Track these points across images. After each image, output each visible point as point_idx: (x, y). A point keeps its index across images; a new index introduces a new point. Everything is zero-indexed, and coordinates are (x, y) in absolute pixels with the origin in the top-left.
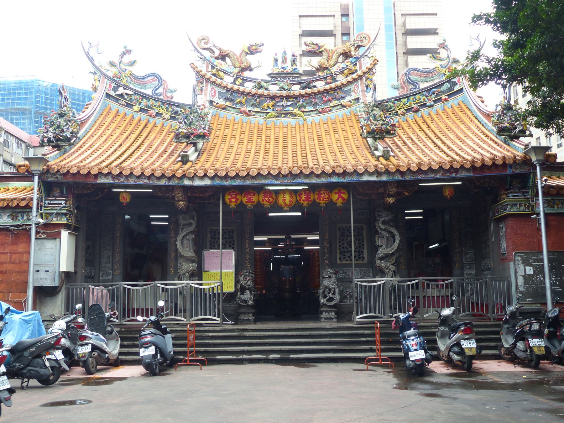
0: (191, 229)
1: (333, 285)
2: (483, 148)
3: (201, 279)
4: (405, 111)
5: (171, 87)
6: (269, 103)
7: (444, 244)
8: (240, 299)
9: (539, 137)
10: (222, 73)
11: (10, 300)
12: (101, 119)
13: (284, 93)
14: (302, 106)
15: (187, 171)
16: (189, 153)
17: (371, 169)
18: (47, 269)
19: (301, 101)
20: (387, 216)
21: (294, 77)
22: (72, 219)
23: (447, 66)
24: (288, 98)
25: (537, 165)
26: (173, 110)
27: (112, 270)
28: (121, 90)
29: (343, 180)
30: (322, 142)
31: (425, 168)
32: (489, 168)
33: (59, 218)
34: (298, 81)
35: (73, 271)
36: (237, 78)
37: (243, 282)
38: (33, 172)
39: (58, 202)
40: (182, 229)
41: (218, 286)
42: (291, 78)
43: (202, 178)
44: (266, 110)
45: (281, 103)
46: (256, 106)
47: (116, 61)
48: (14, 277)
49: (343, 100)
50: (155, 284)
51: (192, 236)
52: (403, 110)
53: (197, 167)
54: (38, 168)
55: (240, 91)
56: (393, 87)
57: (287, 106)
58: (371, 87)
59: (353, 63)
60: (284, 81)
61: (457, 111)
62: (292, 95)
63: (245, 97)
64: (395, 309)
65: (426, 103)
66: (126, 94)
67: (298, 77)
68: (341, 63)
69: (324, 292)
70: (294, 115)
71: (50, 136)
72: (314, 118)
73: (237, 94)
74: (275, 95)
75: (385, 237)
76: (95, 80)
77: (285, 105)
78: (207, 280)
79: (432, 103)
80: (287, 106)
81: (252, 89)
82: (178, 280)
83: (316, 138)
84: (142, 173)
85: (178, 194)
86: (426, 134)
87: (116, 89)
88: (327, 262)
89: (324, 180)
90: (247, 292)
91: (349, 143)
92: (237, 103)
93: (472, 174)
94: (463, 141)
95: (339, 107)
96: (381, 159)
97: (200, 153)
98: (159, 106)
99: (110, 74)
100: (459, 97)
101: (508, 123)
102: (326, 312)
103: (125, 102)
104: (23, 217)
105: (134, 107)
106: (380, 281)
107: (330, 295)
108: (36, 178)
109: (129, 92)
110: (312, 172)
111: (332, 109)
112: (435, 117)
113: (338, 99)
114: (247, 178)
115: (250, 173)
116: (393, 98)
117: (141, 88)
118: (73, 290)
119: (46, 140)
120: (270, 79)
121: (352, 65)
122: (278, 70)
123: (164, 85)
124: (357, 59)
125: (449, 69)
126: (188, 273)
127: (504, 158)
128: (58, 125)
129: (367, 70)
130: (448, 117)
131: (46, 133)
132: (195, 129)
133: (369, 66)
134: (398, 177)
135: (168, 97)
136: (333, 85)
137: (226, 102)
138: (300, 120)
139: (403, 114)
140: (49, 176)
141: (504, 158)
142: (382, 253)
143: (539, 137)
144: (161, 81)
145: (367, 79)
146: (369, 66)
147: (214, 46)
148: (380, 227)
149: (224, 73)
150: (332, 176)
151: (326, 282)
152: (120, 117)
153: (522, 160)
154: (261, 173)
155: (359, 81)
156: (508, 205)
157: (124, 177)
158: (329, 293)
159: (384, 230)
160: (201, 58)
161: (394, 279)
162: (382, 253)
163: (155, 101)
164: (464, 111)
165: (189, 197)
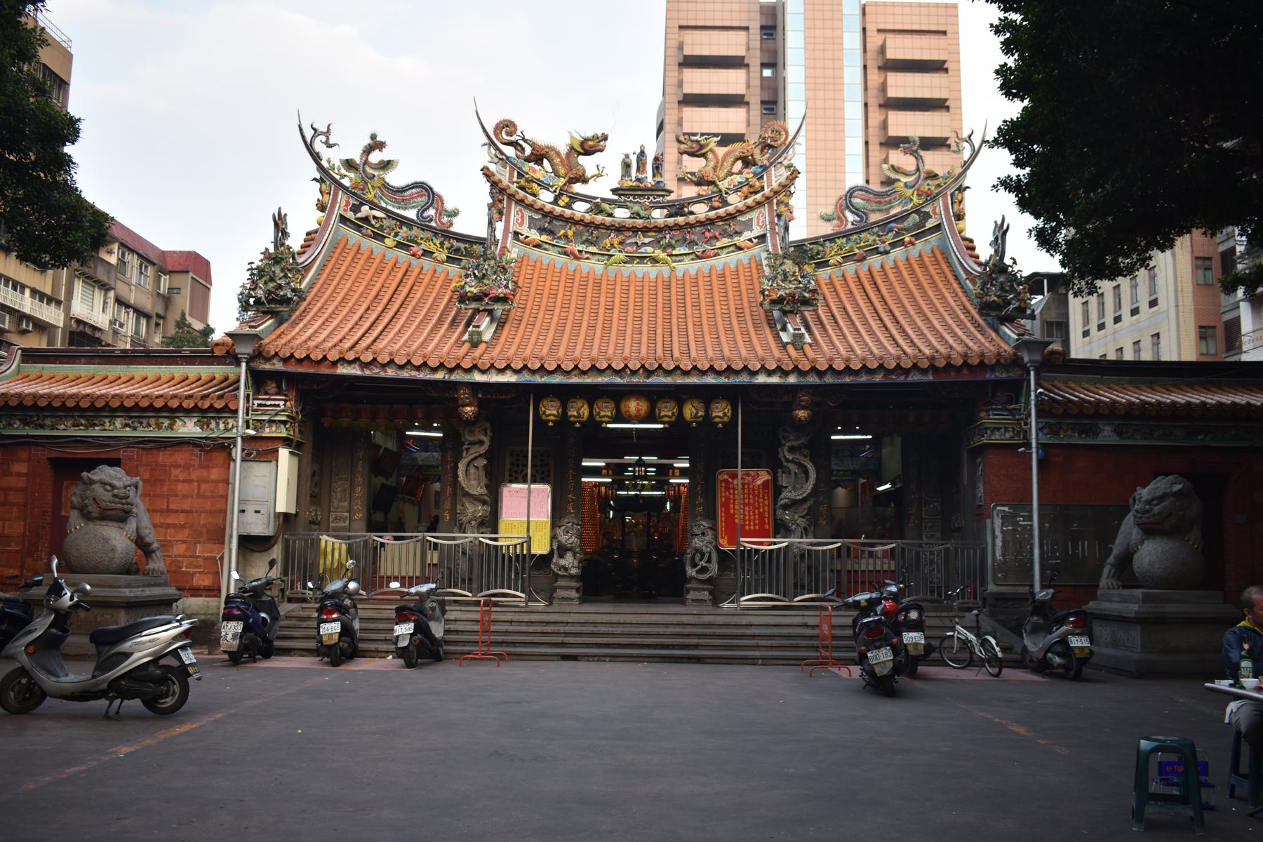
0: (483, 449)
1: (707, 547)
2: (955, 335)
5: (449, 205)
6: (615, 238)
10: (535, 186)
12: (333, 261)
13: (639, 222)
16: (481, 329)
17: (772, 366)
19: (668, 236)
20: (798, 439)
21: (657, 195)
22: (294, 430)
24: (645, 230)
25: (1031, 368)
26: (452, 246)
27: (349, 512)
28: (365, 210)
29: (726, 380)
31: (856, 365)
32: (958, 369)
33: (274, 428)
34: (664, 203)
36: (561, 194)
37: (563, 538)
38: (239, 356)
39: (273, 403)
40: (467, 450)
41: (523, 543)
42: (651, 198)
44: (609, 251)
45: (633, 240)
47: (357, 158)
48: (203, 520)
50: (424, 537)
51: (483, 462)
52: (839, 258)
56: (823, 219)
57: (644, 244)
58: (782, 219)
59: (758, 174)
60: (640, 203)
61: (928, 263)
62: (652, 226)
63: (574, 228)
65: (877, 248)
66: (374, 217)
67: (663, 196)
68: (737, 174)
69: (693, 558)
70: (655, 261)
71: (259, 296)
75: (793, 474)
76: (321, 192)
79: (888, 248)
80: (644, 244)
82: (460, 532)
85: (463, 394)
87: (356, 209)
88: (700, 509)
89: (694, 380)
90: (569, 555)
92: (560, 238)
94: (927, 320)
95: (732, 249)
96: (790, 349)
97: (501, 324)
98: (428, 239)
99: (346, 182)
100: (933, 239)
101: (996, 296)
102: (696, 589)
104: (218, 424)
105: (387, 240)
106: (782, 543)
107: (703, 563)
109: (380, 214)
110: (677, 368)
111: (719, 251)
113: (730, 236)
114: (574, 373)
116: (823, 237)
117: (399, 208)
118: (294, 542)
119: (252, 301)
120: (616, 197)
121: (755, 179)
122: (630, 184)
123: (438, 204)
125: (918, 190)
126: (476, 521)
127: (982, 355)
131: (254, 289)
133: (783, 180)
134: (812, 379)
135: (443, 224)
136: (721, 211)
137: (541, 235)
138: (665, 270)
141: (982, 355)
144: (433, 197)
147: (524, 139)
148: (785, 456)
149: (539, 185)
150: (709, 373)
152: (365, 257)
155: (766, 205)
156: (987, 428)
158: (701, 560)
159: (792, 461)
160: (500, 159)
161: (804, 540)
163: (423, 230)
165: (480, 400)
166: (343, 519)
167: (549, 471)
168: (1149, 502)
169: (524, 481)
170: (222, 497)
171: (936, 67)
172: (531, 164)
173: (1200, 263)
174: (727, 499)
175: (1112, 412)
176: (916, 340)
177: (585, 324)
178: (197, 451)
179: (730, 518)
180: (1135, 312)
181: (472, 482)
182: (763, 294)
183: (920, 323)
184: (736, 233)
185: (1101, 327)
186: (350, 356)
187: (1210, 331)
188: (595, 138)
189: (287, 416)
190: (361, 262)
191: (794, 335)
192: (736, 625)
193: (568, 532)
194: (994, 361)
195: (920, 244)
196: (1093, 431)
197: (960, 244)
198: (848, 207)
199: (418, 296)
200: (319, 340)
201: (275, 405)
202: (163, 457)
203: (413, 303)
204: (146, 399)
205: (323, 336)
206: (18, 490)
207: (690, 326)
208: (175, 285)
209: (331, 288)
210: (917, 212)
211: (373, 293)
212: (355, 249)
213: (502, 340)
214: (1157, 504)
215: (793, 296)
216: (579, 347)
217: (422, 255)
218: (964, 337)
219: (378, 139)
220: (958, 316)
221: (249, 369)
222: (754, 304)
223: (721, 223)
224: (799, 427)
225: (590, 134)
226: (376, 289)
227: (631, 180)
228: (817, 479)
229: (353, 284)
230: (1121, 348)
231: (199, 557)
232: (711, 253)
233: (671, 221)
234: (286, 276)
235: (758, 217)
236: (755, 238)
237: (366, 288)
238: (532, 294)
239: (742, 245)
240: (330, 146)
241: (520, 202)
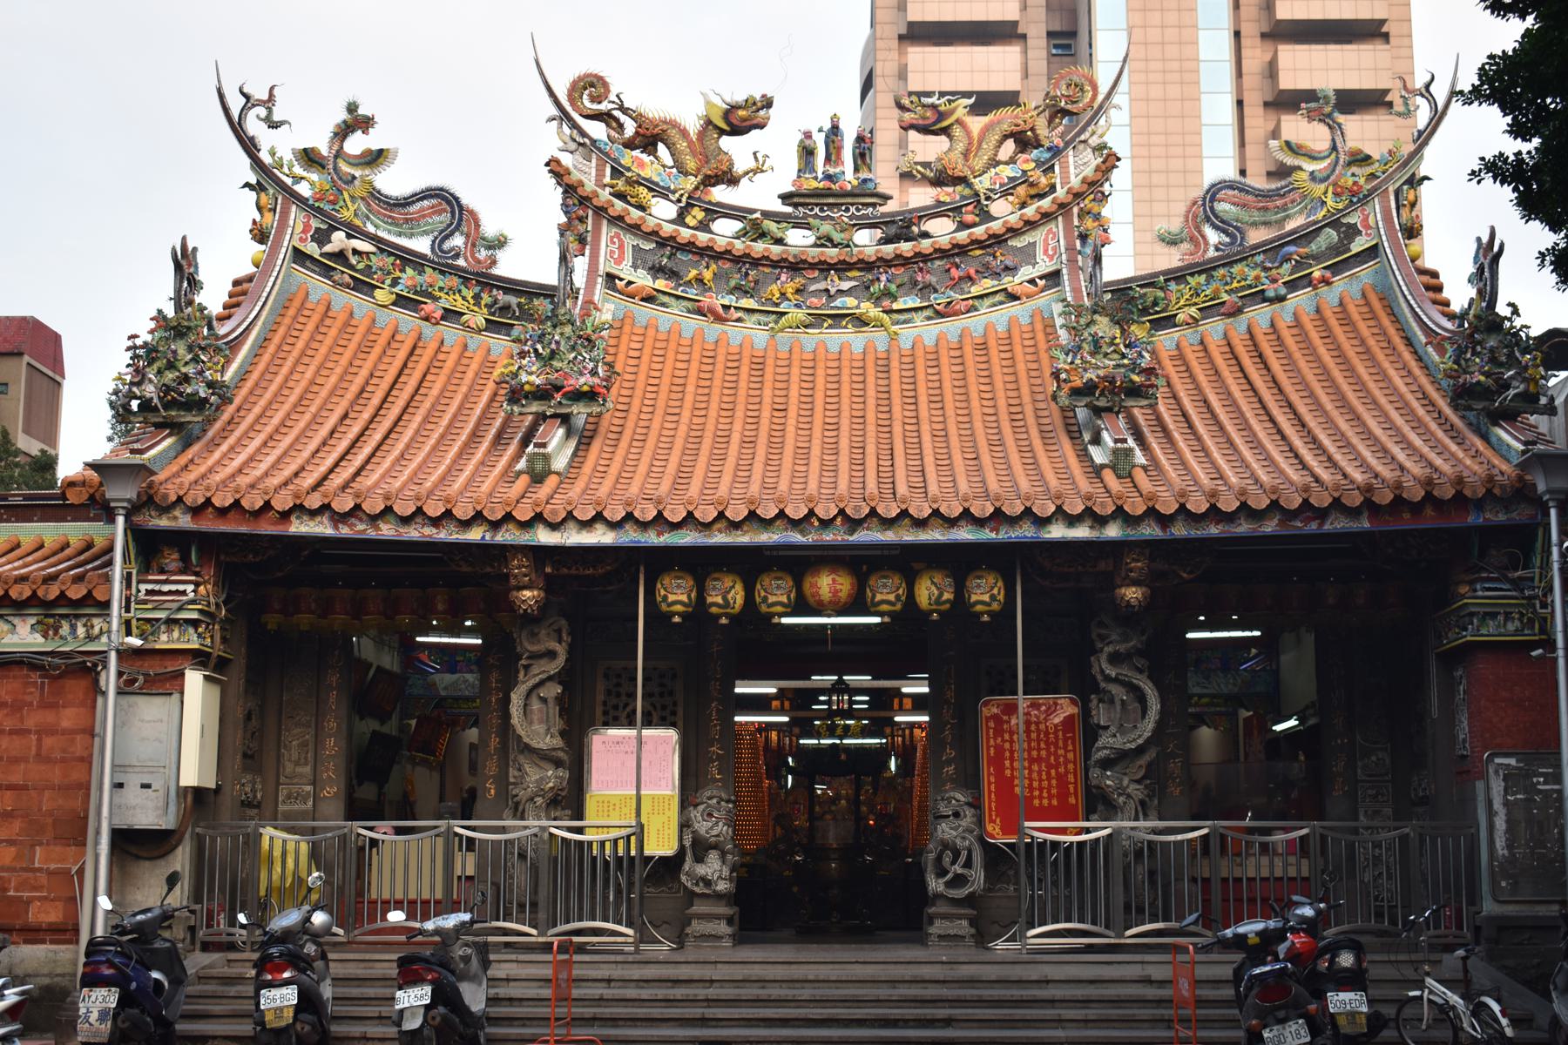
0: (554, 667)
1: (964, 838)
4: (1196, 314)
5: (489, 229)
6: (787, 282)
7: (1312, 721)
11: (37, 865)
12: (282, 330)
13: (832, 253)
14: (887, 294)
15: (547, 503)
16: (549, 449)
17: (1076, 508)
18: (145, 782)
20: (1126, 639)
21: (863, 204)
22: (212, 637)
23: (1328, 177)
24: (842, 267)
25: (1551, 504)
26: (495, 302)
27: (314, 783)
28: (339, 239)
29: (993, 535)
30: (940, 412)
32: (1416, 508)
33: (176, 634)
34: (875, 217)
35: (214, 786)
36: (689, 206)
37: (702, 826)
38: (112, 504)
39: (173, 587)
40: (527, 667)
41: (629, 837)
42: (853, 209)
43: (587, 525)
44: (777, 305)
45: (821, 286)
46: (747, 292)
48: (48, 802)
49: (1011, 279)
50: (449, 828)
51: (554, 690)
52: (1193, 311)
53: (575, 491)
55: (698, 248)
57: (841, 292)
58: (1090, 243)
59: (1044, 163)
60: (832, 219)
61: (1356, 316)
62: (855, 259)
64: (1140, 910)
65: (1263, 291)
66: (355, 252)
67: (874, 205)
69: (939, 859)
70: (861, 322)
71: (148, 395)
73: (690, 256)
74: (805, 261)
76: (259, 208)
79: (1283, 291)
80: (841, 292)
81: (736, 242)
82: (515, 817)
86: (1254, 390)
87: (322, 237)
88: (951, 769)
89: (934, 535)
90: (713, 856)
91: (1020, 416)
93: (1366, 525)
95: (998, 298)
96: (1108, 475)
99: (304, 189)
101: (1483, 374)
102: (944, 917)
103: (351, 276)
104: (73, 628)
105: (378, 293)
106: (1101, 830)
107: (958, 869)
108: (120, 520)
110: (904, 514)
111: (976, 303)
113: (996, 275)
114: (718, 526)
115: (727, 514)
116: (1164, 273)
117: (400, 234)
118: (213, 840)
119: (135, 404)
120: (789, 209)
122: (814, 184)
127: (1459, 481)
128: (169, 360)
131: (138, 384)
133: (1089, 171)
134: (1150, 531)
135: (479, 262)
136: (979, 231)
137: (655, 278)
138: (880, 339)
140: (153, 513)
141: (1459, 481)
142: (1105, 748)
147: (622, 108)
148: (1102, 671)
149: (651, 190)
150: (963, 523)
151: (945, 830)
153: (1512, 486)
154: (758, 512)
155: (1060, 219)
156: (1472, 614)
157: (364, 517)
158: (953, 863)
159: (1116, 680)
160: (580, 144)
161: (1141, 824)
162: (1105, 748)
163: (442, 273)
164: (1375, 317)
167: (675, 704)
169: (631, 723)
170: (82, 759)
172: (637, 153)
174: (999, 750)
177: (736, 438)
178: (35, 677)
179: (1005, 785)
181: (536, 727)
183: (1344, 426)
184: (1007, 268)
188: (750, 103)
189: (200, 611)
190: (333, 332)
191: (1115, 452)
192: (1020, 983)
193: (710, 815)
194: (1481, 492)
195: (1340, 284)
197: (1413, 282)
200: (258, 473)
201: (177, 592)
203: (427, 404)
209: (279, 379)
210: (1335, 224)
212: (321, 309)
213: (587, 468)
216: (727, 479)
217: (443, 318)
218: (1426, 450)
219: (361, 111)
221: (133, 531)
222: (1040, 397)
223: (978, 252)
224: (1128, 617)
225: (740, 98)
227: (816, 178)
228: (1162, 712)
231: (40, 870)
232: (963, 306)
233: (889, 250)
234: (196, 360)
235: (1046, 240)
236: (1041, 278)
239: (1018, 290)
240: (274, 125)
241: (617, 220)
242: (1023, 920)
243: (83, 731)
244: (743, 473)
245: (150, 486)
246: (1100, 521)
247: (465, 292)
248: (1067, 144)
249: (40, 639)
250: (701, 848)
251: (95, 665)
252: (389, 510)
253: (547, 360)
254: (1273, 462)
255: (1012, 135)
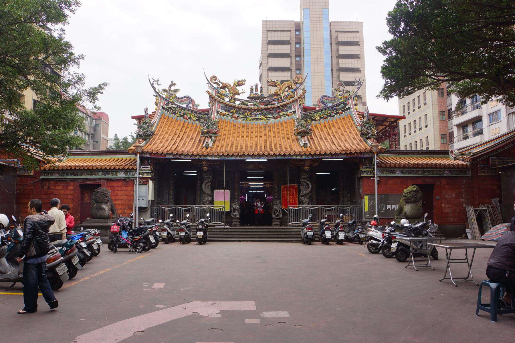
0: (210, 180)
3: (213, 205)
5: (196, 103)
8: (233, 214)
9: (405, 125)
16: (209, 143)
19: (265, 112)
24: (258, 110)
29: (284, 158)
32: (354, 154)
36: (231, 99)
39: (146, 167)
40: (205, 180)
45: (254, 113)
50: (193, 207)
52: (319, 118)
53: (214, 150)
54: (139, 150)
66: (173, 107)
67: (263, 99)
69: (274, 212)
70: (261, 119)
72: (272, 121)
76: (156, 100)
77: (256, 114)
78: (216, 205)
79: (334, 115)
80: (258, 114)
83: (272, 133)
84: (188, 153)
87: (167, 105)
88: (276, 197)
92: (231, 113)
93: (346, 157)
95: (285, 115)
96: (303, 147)
97: (214, 142)
99: (164, 96)
100: (348, 111)
104: (130, 174)
106: (301, 207)
107: (277, 213)
110: (269, 154)
112: (334, 122)
113: (285, 111)
120: (249, 99)
121: (292, 93)
122: (253, 95)
124: (295, 90)
129: (300, 96)
130: (341, 123)
132: (211, 130)
133: (301, 93)
134: (310, 157)
135: (194, 109)
136: (282, 104)
138: (264, 122)
139: (319, 120)
143: (405, 125)
145: (300, 101)
146: (301, 94)
147: (219, 82)
151: (276, 207)
152: (170, 120)
159: (304, 182)
161: (308, 206)
163: (188, 111)
165: (209, 165)
166: (167, 202)
168: (407, 193)
169: (222, 189)
170: (132, 195)
171: (356, 44)
172: (222, 89)
173: (441, 113)
174: (284, 193)
175: (400, 167)
176: (341, 145)
177: (240, 140)
178: (124, 182)
179: (285, 200)
180: (420, 129)
181: (207, 190)
182: (295, 131)
183: (343, 139)
185: (410, 134)
186: (170, 152)
187: (444, 136)
188: (242, 81)
190: (170, 122)
191: (304, 144)
194: (364, 151)
195: (344, 113)
196: (393, 172)
197: (355, 113)
198: (321, 102)
199: (188, 132)
200: (160, 147)
201: (147, 168)
202: (114, 184)
203: (187, 134)
204: (117, 166)
205: (161, 146)
206: (71, 194)
207: (273, 141)
208: (97, 123)
209: (161, 130)
210: (343, 103)
211: (174, 132)
212: (167, 117)
213: (215, 146)
214: (409, 194)
215: (304, 131)
216: (239, 148)
217: (188, 119)
218: (356, 144)
219: (174, 82)
220: (354, 137)
221: (140, 158)
222: (292, 133)
223: (282, 107)
224: (306, 172)
225: (240, 80)
226: (175, 130)
228: (312, 187)
229: (168, 129)
230: (428, 137)
232: (279, 117)
234: (148, 128)
237: (172, 130)
238: (223, 131)
240: (159, 85)
242: (288, 222)
243: (132, 191)
244: (241, 147)
245: (143, 150)
246: (301, 155)
247: (192, 114)
248: (297, 88)
249: (125, 175)
250: (234, 210)
251: (134, 180)
252: (182, 154)
253: (208, 127)
254: (331, 146)
255: (287, 87)
